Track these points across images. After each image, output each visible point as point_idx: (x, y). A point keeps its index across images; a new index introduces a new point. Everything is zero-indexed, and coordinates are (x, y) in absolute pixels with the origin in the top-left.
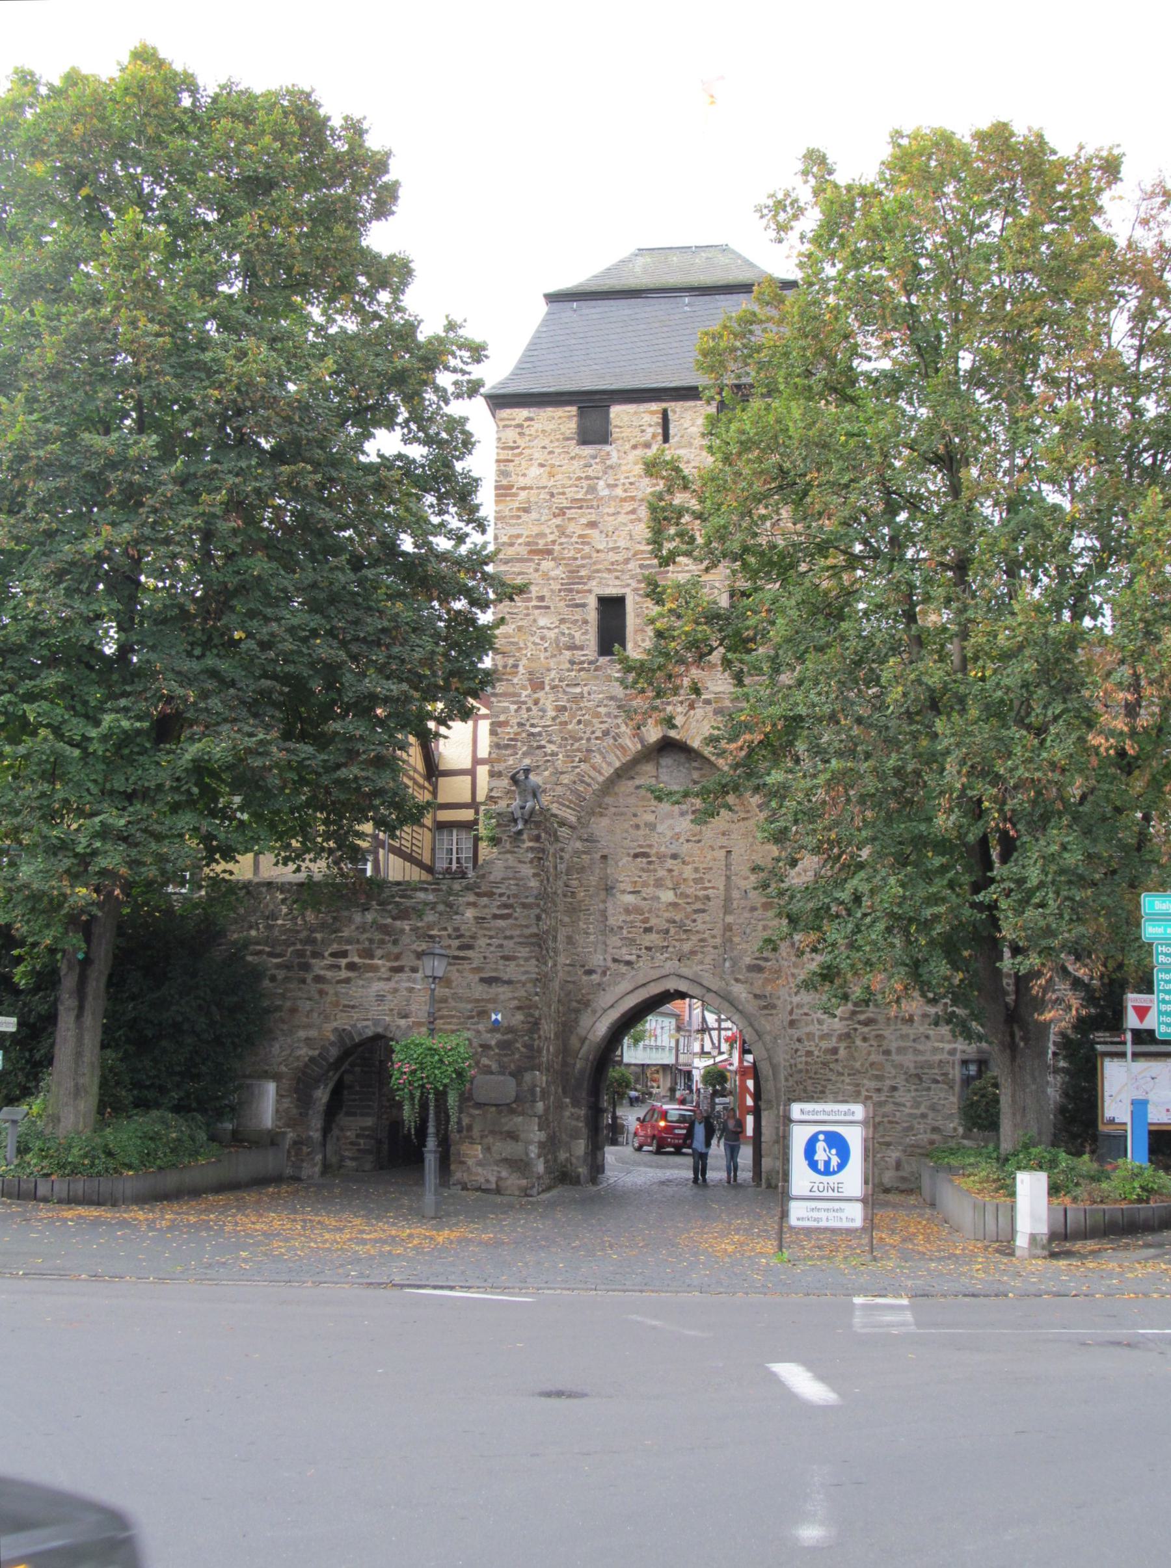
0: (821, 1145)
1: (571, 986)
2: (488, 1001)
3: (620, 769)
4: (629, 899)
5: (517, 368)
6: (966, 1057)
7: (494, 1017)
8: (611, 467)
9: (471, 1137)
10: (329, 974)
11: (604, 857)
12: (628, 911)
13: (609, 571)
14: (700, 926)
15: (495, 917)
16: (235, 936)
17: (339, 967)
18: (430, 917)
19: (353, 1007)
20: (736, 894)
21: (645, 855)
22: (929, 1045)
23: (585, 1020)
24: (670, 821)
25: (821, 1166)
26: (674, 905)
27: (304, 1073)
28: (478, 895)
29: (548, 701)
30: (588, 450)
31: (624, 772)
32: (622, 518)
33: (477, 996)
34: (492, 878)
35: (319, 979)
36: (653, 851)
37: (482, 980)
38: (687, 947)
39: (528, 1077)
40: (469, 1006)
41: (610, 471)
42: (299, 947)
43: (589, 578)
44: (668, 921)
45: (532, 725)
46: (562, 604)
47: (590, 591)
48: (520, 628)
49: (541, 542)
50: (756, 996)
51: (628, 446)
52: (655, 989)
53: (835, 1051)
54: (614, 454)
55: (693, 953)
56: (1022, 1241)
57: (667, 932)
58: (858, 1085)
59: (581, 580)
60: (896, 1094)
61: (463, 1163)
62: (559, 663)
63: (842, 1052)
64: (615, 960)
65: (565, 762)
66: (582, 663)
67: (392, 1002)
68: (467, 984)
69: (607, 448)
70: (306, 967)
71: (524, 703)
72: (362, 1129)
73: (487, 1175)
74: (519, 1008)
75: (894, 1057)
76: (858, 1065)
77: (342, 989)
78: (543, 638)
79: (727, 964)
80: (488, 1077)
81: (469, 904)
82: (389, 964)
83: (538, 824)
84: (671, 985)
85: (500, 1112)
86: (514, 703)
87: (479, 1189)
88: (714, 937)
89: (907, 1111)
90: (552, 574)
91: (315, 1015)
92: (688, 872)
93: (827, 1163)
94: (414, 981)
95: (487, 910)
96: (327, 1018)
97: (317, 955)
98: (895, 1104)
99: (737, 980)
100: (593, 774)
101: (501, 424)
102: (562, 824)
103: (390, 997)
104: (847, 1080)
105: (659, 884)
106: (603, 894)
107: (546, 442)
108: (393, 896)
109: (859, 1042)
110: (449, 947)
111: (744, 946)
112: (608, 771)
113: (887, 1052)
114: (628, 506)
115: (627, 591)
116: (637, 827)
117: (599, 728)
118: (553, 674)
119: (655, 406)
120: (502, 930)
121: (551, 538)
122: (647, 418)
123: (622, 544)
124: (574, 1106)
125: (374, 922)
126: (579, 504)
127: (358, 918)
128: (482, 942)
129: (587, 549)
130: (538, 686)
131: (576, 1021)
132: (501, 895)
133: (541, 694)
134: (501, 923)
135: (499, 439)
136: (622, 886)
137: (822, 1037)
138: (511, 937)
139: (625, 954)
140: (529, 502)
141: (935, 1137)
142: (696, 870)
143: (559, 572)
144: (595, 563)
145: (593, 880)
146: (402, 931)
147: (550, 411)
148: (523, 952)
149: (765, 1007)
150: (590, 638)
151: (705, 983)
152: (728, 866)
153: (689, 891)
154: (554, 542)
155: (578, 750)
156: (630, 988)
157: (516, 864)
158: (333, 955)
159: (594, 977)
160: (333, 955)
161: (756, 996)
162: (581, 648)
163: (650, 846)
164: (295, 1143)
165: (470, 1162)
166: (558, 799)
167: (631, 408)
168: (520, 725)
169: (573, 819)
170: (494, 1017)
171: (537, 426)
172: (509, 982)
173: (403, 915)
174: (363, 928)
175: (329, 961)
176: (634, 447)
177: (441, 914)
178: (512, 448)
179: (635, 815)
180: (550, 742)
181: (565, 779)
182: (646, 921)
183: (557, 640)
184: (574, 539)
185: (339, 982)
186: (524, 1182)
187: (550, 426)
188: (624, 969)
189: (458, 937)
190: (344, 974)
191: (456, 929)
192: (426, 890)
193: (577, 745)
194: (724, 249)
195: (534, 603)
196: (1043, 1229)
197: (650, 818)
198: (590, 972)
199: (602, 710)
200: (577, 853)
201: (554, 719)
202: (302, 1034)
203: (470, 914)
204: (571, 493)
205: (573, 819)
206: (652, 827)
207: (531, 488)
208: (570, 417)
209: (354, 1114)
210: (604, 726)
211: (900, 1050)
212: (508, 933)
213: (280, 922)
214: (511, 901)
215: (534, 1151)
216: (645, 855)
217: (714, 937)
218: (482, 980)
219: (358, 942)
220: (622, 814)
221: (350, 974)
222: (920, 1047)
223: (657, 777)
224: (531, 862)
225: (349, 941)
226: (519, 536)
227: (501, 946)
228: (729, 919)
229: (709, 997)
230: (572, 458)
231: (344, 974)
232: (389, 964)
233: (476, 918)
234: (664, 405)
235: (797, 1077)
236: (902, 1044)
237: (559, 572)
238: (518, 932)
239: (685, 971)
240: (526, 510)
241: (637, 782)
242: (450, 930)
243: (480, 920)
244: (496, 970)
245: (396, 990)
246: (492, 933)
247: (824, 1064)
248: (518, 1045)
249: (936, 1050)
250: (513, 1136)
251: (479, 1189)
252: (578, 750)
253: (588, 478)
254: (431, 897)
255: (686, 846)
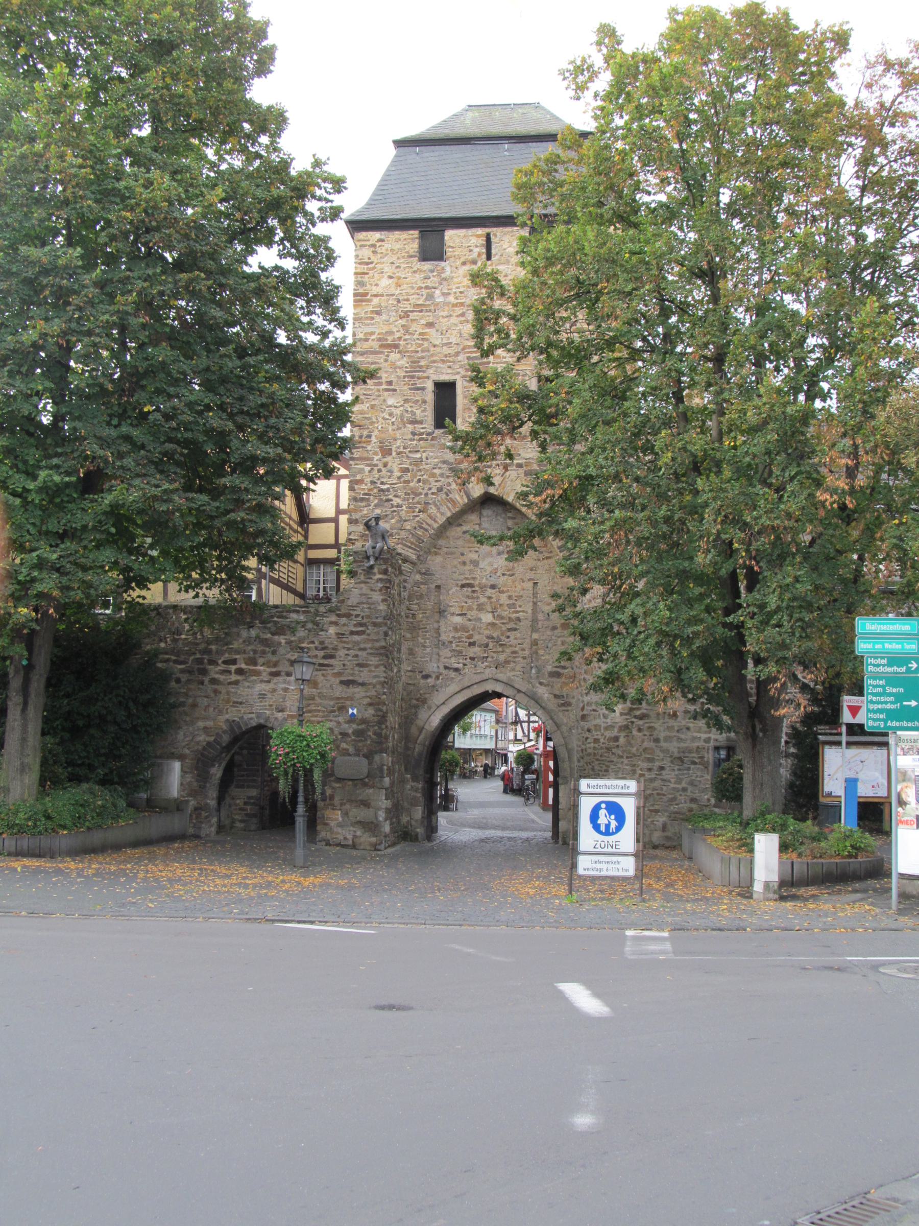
0: (603, 812)
1: (412, 688)
2: (347, 699)
3: (451, 517)
4: (458, 620)
5: (371, 199)
6: (718, 744)
7: (351, 711)
8: (445, 279)
9: (333, 805)
10: (222, 678)
11: (438, 587)
12: (456, 629)
13: (443, 361)
14: (513, 641)
15: (352, 633)
16: (148, 647)
17: (229, 672)
18: (301, 633)
19: (241, 703)
20: (540, 617)
21: (470, 585)
22: (689, 734)
23: (423, 714)
24: (490, 559)
25: (603, 828)
26: (493, 625)
27: (202, 755)
28: (338, 615)
29: (394, 464)
30: (427, 266)
31: (453, 521)
32: (454, 320)
33: (338, 694)
34: (350, 603)
35: (214, 681)
36: (477, 582)
37: (342, 682)
38: (502, 658)
39: (377, 758)
40: (332, 703)
41: (445, 283)
42: (198, 656)
43: (428, 367)
44: (488, 637)
45: (382, 483)
46: (406, 387)
47: (428, 378)
48: (373, 407)
49: (390, 338)
50: (556, 696)
51: (458, 263)
52: (477, 690)
53: (616, 739)
54: (448, 269)
55: (507, 662)
56: (758, 887)
57: (487, 645)
58: (634, 765)
59: (421, 369)
60: (664, 772)
61: (327, 824)
62: (403, 434)
63: (622, 740)
64: (446, 668)
65: (407, 512)
66: (422, 434)
67: (271, 699)
68: (330, 685)
69: (443, 264)
70: (204, 672)
71: (376, 465)
72: (250, 798)
73: (346, 834)
74: (370, 704)
75: (663, 744)
76: (634, 750)
77: (232, 689)
78: (391, 414)
79: (533, 671)
80: (347, 758)
81: (331, 623)
82: (269, 670)
83: (386, 561)
84: (490, 687)
85: (356, 785)
86: (367, 465)
87: (339, 845)
88: (523, 650)
89: (672, 785)
90: (399, 364)
91: (211, 709)
92: (504, 599)
93: (608, 826)
94: (289, 683)
95: (345, 628)
96: (220, 712)
97: (213, 662)
98: (663, 780)
99: (541, 684)
100: (430, 521)
101: (359, 244)
102: (405, 560)
103: (269, 696)
104: (626, 761)
105: (481, 608)
106: (437, 616)
107: (394, 259)
108: (272, 617)
109: (635, 732)
110: (316, 656)
111: (547, 657)
112: (441, 520)
113: (657, 740)
114: (459, 311)
115: (457, 377)
116: (464, 563)
117: (435, 486)
118: (399, 443)
119: (480, 231)
120: (357, 643)
121: (398, 335)
122: (474, 240)
123: (454, 340)
124: (413, 781)
125: (258, 637)
126: (420, 308)
127: (244, 634)
128: (342, 653)
129: (426, 344)
130: (386, 452)
131: (416, 714)
132: (357, 616)
133: (388, 459)
134: (356, 638)
135: (357, 256)
136: (452, 610)
137: (606, 728)
138: (365, 649)
139: (454, 663)
140: (380, 306)
141: (694, 806)
142: (510, 597)
143: (403, 362)
144: (432, 355)
145: (430, 605)
146: (280, 643)
147: (397, 234)
148: (374, 661)
149: (563, 705)
150: (427, 414)
151: (517, 686)
152: (535, 595)
153: (505, 614)
154: (400, 339)
155: (418, 503)
156: (457, 689)
157: (369, 592)
158: (225, 662)
159: (429, 680)
160: (225, 662)
161: (556, 696)
162: (421, 422)
163: (474, 579)
164: (196, 809)
165: (332, 824)
166: (401, 541)
167: (462, 232)
168: (373, 482)
169: (414, 557)
170: (351, 711)
171: (387, 246)
172: (363, 684)
173: (280, 631)
174: (248, 641)
175: (222, 667)
176: (464, 263)
177: (310, 631)
178: (367, 264)
179: (462, 554)
180: (396, 496)
181: (408, 526)
182: (470, 637)
183: (402, 416)
184: (416, 336)
185: (230, 683)
186: (374, 840)
187: (397, 246)
188: (453, 674)
189: (323, 649)
190: (234, 677)
191: (322, 643)
192: (298, 612)
193: (417, 499)
194: (537, 106)
195: (384, 387)
196: (775, 878)
197: (474, 556)
198: (426, 677)
199: (437, 471)
200: (417, 584)
201: (399, 478)
202: (201, 724)
203: (332, 630)
204: (414, 299)
205: (414, 557)
206: (475, 563)
207: (382, 295)
208: (413, 239)
209: (242, 787)
210: (439, 484)
211: (668, 739)
212: (362, 646)
213: (183, 636)
214: (365, 621)
215: (382, 815)
216: (470, 585)
217: (523, 650)
218: (342, 682)
219: (244, 652)
220: (452, 553)
221: (239, 678)
222: (683, 736)
223: (480, 525)
224: (380, 590)
225: (238, 652)
226: (372, 333)
227: (357, 656)
228: (535, 636)
229: (519, 697)
230: (415, 272)
231: (234, 677)
232: (269, 670)
233: (337, 634)
234: (488, 230)
235: (587, 759)
236: (668, 734)
237: (403, 362)
238: (369, 645)
239: (501, 676)
240: (378, 313)
241: (465, 528)
242: (317, 643)
243: (340, 635)
244: (352, 675)
245: (274, 690)
246: (350, 646)
247: (607, 749)
248: (370, 733)
249: (694, 739)
250: (366, 804)
251: (339, 845)
252: (418, 503)
253: (427, 288)
254: (302, 618)
255: (502, 578)
